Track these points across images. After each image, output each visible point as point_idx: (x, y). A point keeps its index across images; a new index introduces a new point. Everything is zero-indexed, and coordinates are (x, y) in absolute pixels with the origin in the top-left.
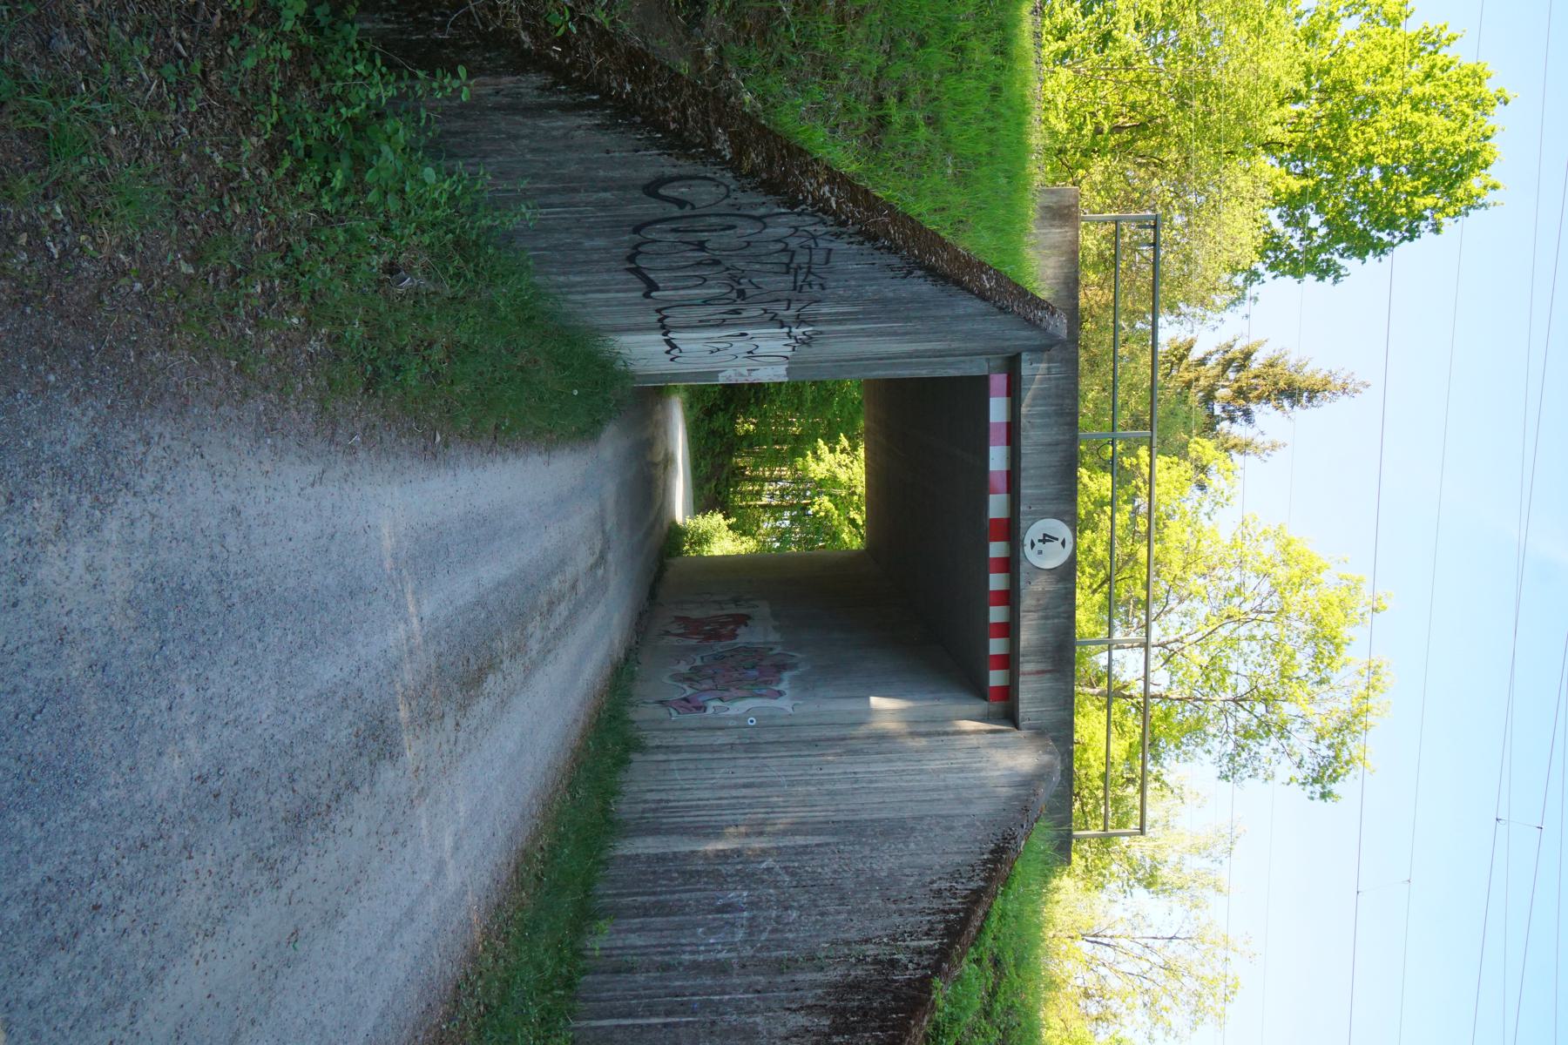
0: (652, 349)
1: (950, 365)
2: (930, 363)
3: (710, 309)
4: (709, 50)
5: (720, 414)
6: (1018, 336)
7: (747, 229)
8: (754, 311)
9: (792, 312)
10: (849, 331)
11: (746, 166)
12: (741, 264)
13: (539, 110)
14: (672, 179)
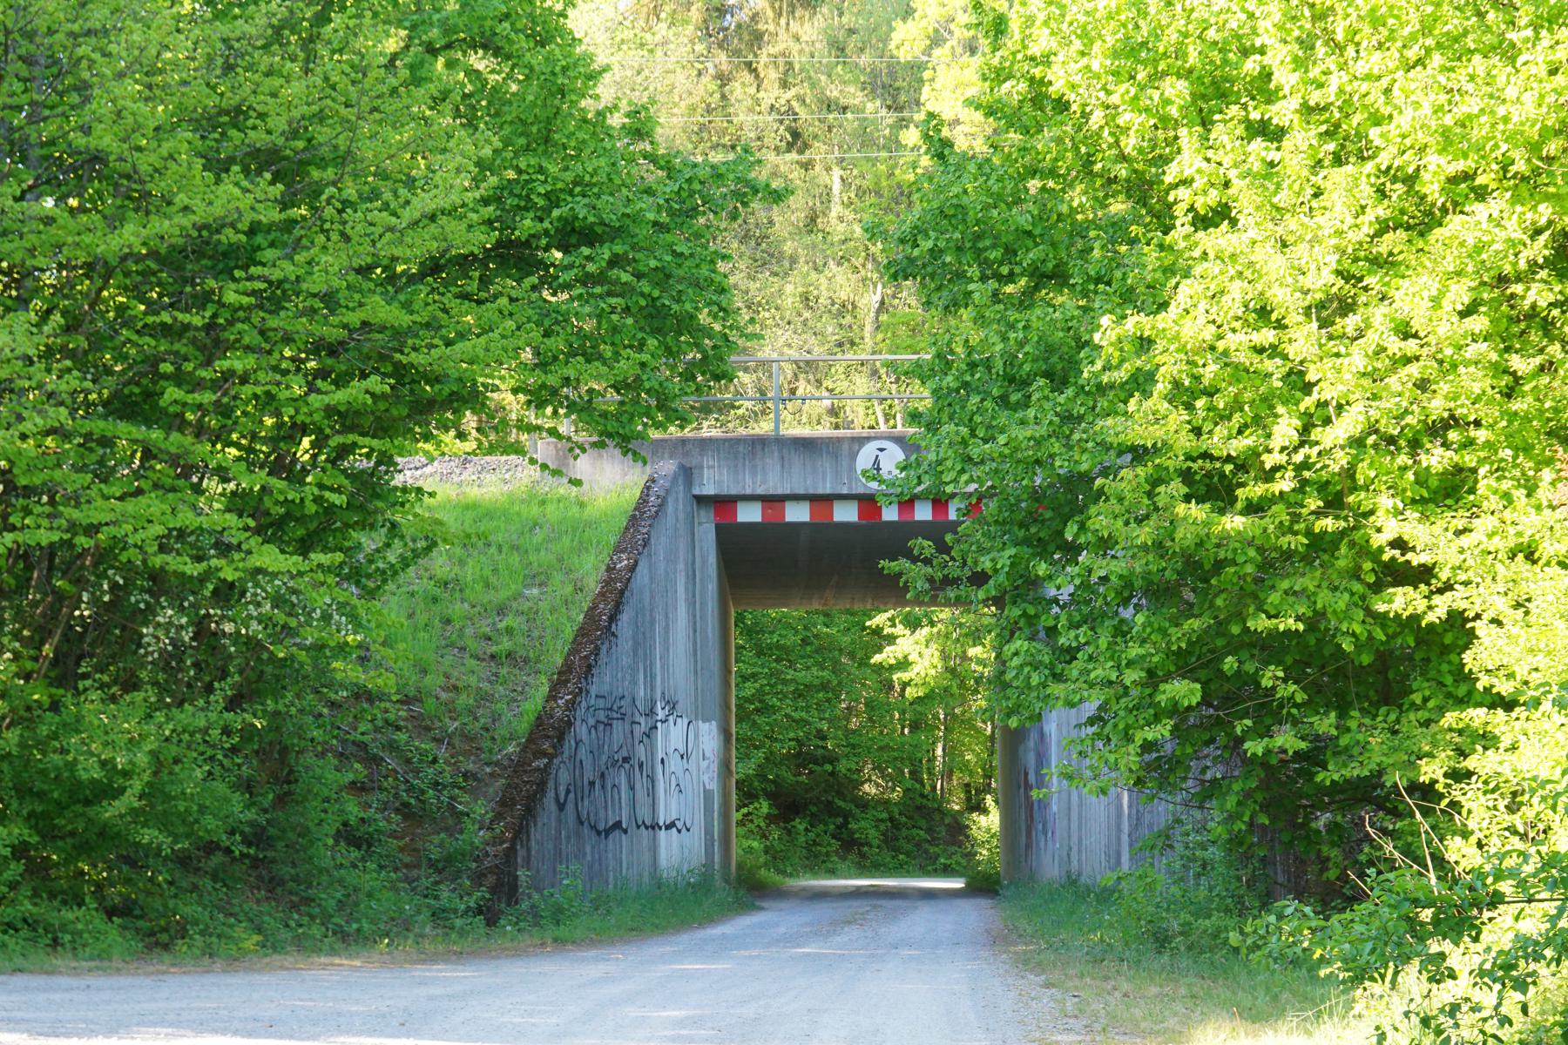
0: (675, 845)
1: (704, 562)
2: (702, 580)
3: (638, 786)
4: (488, 770)
5: (853, 826)
6: (677, 507)
7: (583, 753)
8: (641, 752)
9: (642, 720)
10: (662, 667)
11: (551, 751)
12: (604, 758)
13: (529, 850)
14: (557, 795)
